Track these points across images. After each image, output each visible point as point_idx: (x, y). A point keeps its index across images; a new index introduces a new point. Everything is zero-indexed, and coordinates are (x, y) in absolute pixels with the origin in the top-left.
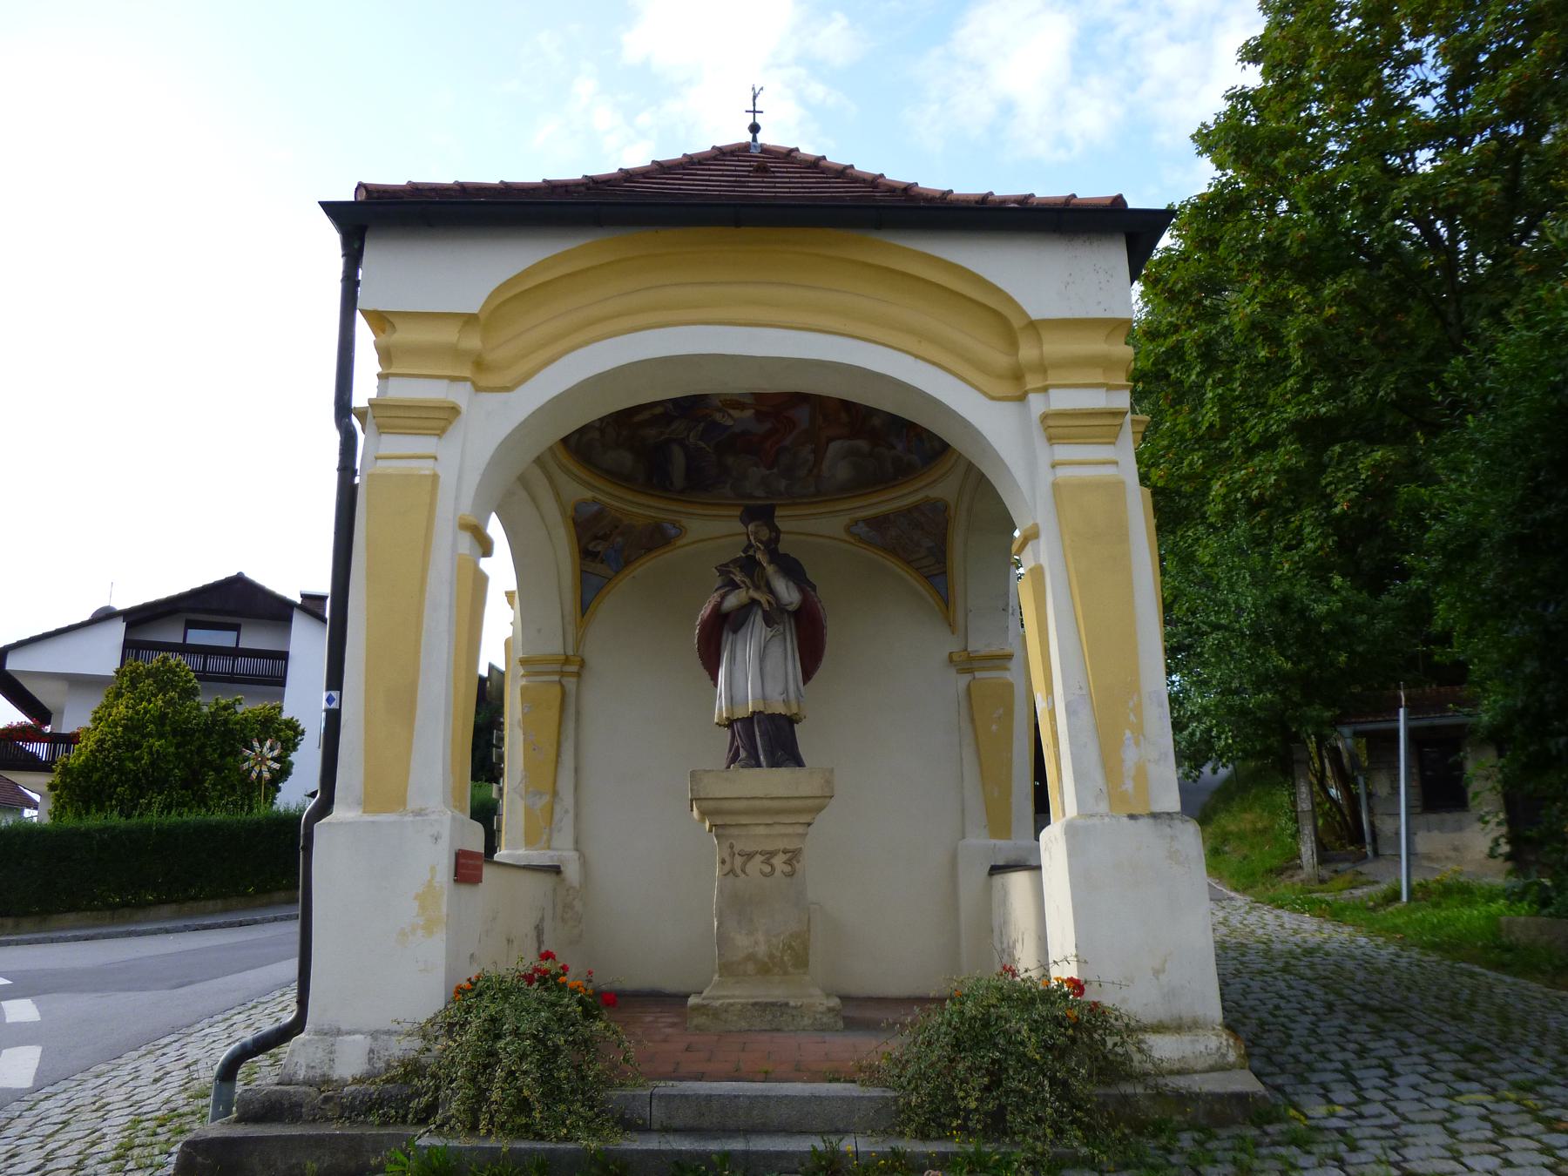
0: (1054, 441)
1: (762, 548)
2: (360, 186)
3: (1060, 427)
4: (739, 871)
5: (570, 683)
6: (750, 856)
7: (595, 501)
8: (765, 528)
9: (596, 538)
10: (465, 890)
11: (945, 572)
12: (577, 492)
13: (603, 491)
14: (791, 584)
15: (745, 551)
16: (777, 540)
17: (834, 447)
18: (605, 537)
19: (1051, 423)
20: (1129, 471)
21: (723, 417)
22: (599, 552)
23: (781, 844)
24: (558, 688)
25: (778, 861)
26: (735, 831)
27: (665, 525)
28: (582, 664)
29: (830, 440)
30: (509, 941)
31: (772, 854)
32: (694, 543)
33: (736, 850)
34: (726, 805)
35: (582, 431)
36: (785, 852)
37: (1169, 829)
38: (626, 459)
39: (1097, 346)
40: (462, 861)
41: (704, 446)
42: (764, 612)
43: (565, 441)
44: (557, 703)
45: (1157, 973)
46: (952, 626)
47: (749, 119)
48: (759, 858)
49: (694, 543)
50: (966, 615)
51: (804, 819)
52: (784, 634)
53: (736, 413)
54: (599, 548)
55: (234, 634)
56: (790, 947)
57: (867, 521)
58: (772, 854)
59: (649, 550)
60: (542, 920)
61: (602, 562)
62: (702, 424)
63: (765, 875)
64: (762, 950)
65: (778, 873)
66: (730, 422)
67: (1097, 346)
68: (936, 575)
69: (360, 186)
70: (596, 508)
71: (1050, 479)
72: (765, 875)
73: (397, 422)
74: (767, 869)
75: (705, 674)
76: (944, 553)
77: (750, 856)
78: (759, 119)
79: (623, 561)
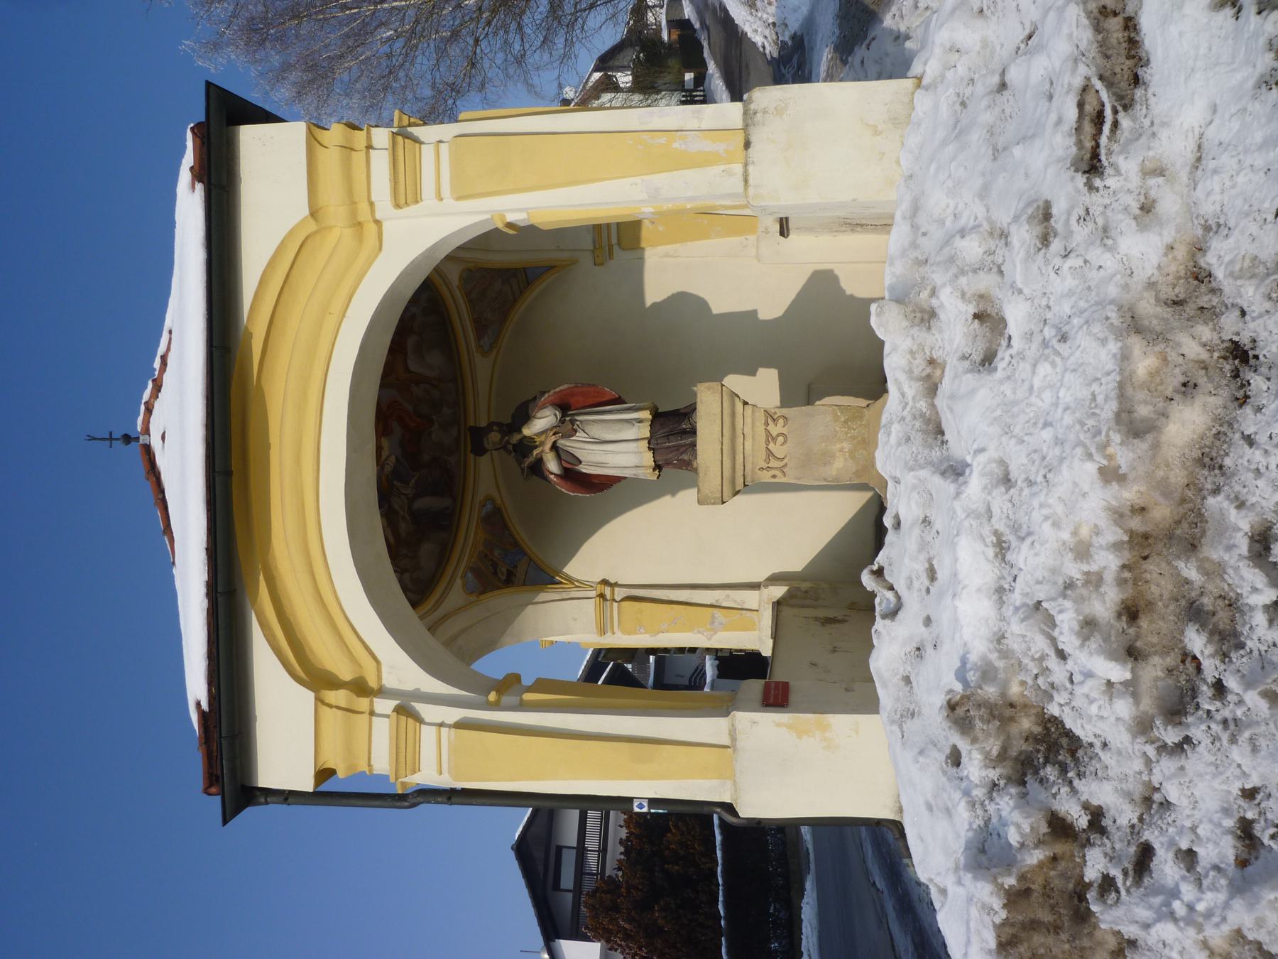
0: (419, 199)
1: (507, 438)
2: (206, 792)
3: (406, 192)
4: (782, 464)
5: (620, 593)
6: (769, 453)
7: (464, 577)
8: (490, 436)
9: (495, 573)
10: (793, 697)
11: (524, 269)
12: (457, 595)
13: (457, 564)
14: (539, 415)
15: (509, 452)
16: (499, 424)
17: (413, 366)
18: (495, 565)
19: (402, 201)
20: (446, 131)
21: (388, 464)
22: (507, 570)
23: (760, 428)
24: (624, 604)
25: (775, 430)
26: (749, 467)
27: (483, 514)
28: (605, 582)
29: (407, 370)
30: (834, 650)
31: (768, 433)
32: (499, 491)
33: (765, 465)
34: (727, 473)
35: (405, 589)
36: (767, 424)
37: (758, 115)
38: (427, 549)
39: (330, 159)
40: (771, 701)
41: (413, 481)
42: (562, 437)
43: (414, 605)
44: (637, 604)
45: (876, 132)
46: (574, 262)
47: (118, 445)
48: (771, 446)
49: (499, 491)
50: (561, 250)
51: (739, 405)
52: (581, 421)
53: (385, 453)
54: (504, 570)
55: (564, 851)
56: (845, 422)
57: (479, 337)
58: (768, 433)
59: (505, 526)
60: (816, 619)
61: (515, 567)
62: (395, 483)
63: (785, 441)
64: (847, 446)
65: (784, 431)
66: (393, 459)
67: (330, 159)
68: (526, 276)
69: (206, 792)
70: (470, 575)
71: (452, 201)
72: (785, 441)
73: (410, 750)
74: (781, 439)
75: (616, 487)
76: (507, 270)
77: (770, 453)
78: (117, 435)
79: (516, 548)
